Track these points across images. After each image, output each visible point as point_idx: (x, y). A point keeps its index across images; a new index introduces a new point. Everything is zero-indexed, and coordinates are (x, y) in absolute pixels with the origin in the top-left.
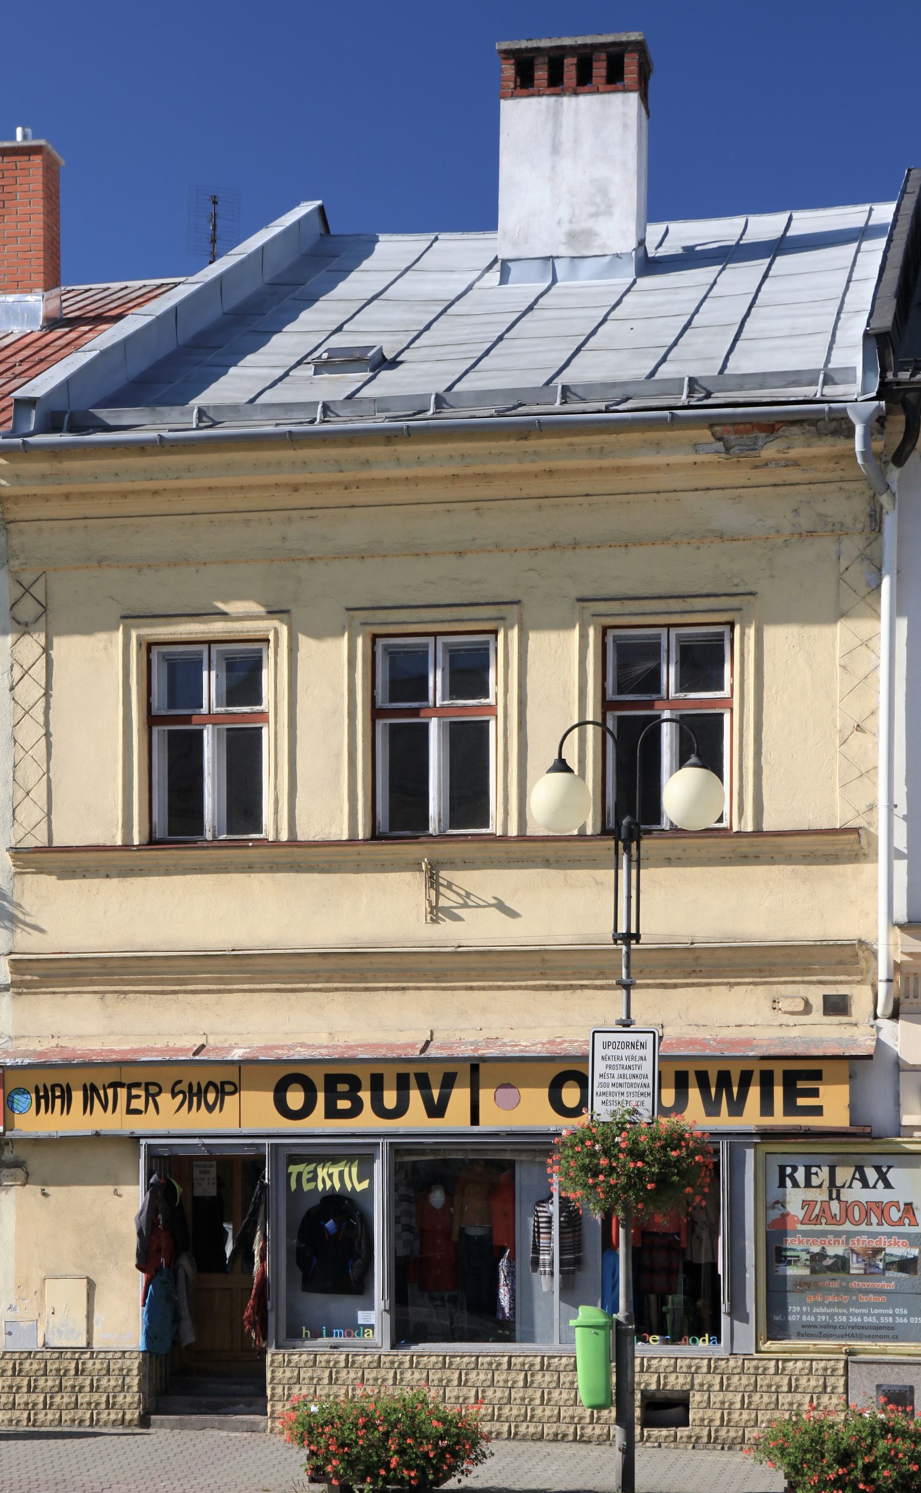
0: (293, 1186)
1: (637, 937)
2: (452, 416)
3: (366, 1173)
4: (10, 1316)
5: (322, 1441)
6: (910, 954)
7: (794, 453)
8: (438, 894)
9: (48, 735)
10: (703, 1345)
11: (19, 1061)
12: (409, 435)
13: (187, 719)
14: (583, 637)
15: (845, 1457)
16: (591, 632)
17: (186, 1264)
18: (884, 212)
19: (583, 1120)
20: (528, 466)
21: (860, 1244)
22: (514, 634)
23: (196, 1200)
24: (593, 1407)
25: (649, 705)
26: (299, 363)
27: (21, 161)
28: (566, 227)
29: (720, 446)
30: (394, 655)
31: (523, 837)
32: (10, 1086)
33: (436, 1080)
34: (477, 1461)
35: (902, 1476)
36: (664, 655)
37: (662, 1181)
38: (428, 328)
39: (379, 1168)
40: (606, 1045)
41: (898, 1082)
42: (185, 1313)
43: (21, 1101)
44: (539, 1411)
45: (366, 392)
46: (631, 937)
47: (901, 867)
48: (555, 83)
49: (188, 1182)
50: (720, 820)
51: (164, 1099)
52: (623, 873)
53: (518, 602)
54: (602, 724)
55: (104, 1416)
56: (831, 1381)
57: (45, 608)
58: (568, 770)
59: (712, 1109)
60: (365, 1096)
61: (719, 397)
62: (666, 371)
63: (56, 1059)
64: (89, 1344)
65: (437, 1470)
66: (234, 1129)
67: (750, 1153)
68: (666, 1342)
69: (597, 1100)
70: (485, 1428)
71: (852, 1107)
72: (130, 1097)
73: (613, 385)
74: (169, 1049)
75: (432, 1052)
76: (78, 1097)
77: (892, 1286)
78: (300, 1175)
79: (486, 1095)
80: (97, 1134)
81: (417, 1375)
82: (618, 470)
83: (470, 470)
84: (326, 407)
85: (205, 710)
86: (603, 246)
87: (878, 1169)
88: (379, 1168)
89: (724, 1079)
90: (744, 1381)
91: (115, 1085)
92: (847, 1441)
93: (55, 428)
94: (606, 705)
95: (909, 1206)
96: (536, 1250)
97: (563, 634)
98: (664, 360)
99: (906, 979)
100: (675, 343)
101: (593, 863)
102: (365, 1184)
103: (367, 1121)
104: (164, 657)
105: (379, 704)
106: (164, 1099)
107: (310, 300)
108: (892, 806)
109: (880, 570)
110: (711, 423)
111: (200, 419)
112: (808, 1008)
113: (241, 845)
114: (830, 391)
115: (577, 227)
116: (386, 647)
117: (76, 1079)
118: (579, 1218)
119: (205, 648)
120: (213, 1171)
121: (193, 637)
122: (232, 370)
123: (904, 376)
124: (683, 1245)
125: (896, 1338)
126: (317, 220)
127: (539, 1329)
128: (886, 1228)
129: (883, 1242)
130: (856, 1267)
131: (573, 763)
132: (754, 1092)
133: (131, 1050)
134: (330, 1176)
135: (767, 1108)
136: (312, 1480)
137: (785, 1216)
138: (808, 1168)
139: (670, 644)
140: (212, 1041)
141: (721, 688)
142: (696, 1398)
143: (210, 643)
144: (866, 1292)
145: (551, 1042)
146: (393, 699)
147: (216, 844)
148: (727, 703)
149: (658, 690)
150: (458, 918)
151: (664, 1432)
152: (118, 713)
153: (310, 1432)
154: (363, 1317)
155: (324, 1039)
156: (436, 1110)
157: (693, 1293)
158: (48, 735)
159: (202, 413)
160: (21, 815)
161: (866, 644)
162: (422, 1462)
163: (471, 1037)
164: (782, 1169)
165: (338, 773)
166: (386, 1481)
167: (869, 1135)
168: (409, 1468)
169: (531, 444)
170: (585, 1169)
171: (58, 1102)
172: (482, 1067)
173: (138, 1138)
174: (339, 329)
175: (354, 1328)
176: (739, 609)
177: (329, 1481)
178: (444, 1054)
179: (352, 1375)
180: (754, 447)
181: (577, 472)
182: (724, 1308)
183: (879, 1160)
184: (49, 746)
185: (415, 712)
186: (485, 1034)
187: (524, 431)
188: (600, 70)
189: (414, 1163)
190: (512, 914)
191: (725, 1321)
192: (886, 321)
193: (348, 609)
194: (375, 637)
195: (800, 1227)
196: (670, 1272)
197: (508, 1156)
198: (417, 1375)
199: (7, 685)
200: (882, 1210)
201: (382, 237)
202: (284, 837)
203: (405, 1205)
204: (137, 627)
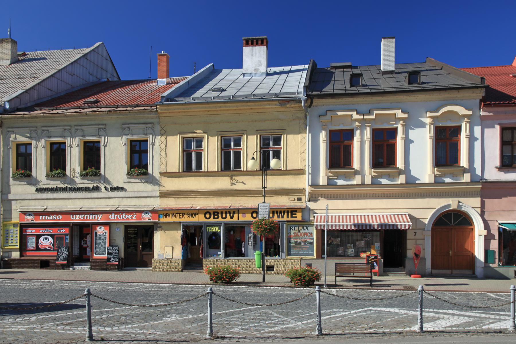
0: (207, 231)
1: (266, 188)
2: (235, 99)
3: (220, 229)
4: (159, 253)
5: (212, 274)
6: (312, 191)
7: (292, 106)
8: (232, 181)
9: (166, 153)
10: (277, 257)
11: (161, 209)
12: (228, 102)
13: (190, 151)
14: (257, 137)
15: (300, 275)
16: (258, 136)
17: (189, 244)
18: (307, 66)
19: (257, 219)
20: (248, 108)
21: (303, 240)
22: (245, 136)
23: (191, 233)
24: (258, 268)
25: (268, 148)
26: (209, 90)
27: (163, 57)
28: (254, 68)
29: (280, 104)
30: (225, 140)
31: (247, 171)
32: (159, 214)
33: (232, 212)
34: (239, 277)
35: (310, 278)
36: (270, 140)
37: (270, 229)
38: (231, 84)
39: (222, 228)
40: (261, 206)
41: (309, 212)
42: (189, 252)
43: (161, 216)
44: (249, 269)
45: (220, 95)
46: (265, 188)
47: (310, 176)
48: (252, 44)
49: (190, 230)
50: (280, 168)
51: (185, 216)
52: (264, 177)
53: (246, 131)
54: (260, 151)
55: (175, 270)
56: (298, 263)
57: (166, 132)
58: (254, 159)
59: (278, 217)
60: (220, 215)
61: (280, 96)
62: (271, 92)
63: (167, 209)
64: (173, 258)
65: (232, 279)
66: (197, 221)
67: (285, 225)
68: (270, 257)
69: (259, 216)
70: (240, 272)
71: (302, 217)
72: (180, 216)
73: (262, 94)
74: (186, 207)
75: (231, 208)
76: (171, 215)
77: (308, 247)
78: (208, 229)
79: (240, 215)
80: (174, 222)
81: (228, 263)
82: (263, 108)
83: (238, 108)
84: (214, 97)
85: (193, 149)
86: (260, 71)
87: (306, 227)
88: (222, 228)
89: (281, 212)
90: (284, 263)
91: (177, 213)
92: (301, 273)
93: (168, 101)
94: (261, 148)
95: (311, 233)
96: (249, 241)
97: (254, 136)
98: (270, 90)
99: (311, 195)
100: (272, 87)
101: (259, 175)
102: (220, 230)
103: (220, 219)
104: (186, 140)
105: (222, 148)
106: (185, 216)
107: (211, 80)
108: (309, 166)
109: (306, 125)
110: (278, 100)
111: (192, 100)
112: (295, 200)
113: (199, 172)
114: (298, 95)
115: (256, 68)
116: (223, 138)
117: (171, 212)
118: (256, 236)
119: (193, 138)
120: (194, 228)
121: (191, 137)
122: (198, 91)
123: (310, 93)
124: (274, 240)
125: (309, 256)
126: (212, 68)
127: (249, 254)
128: (307, 237)
129: (307, 239)
130: (302, 244)
131: (255, 158)
132: (286, 214)
133: (180, 208)
134: (214, 229)
135: (288, 217)
136: (210, 280)
137: (291, 235)
138: (295, 227)
139: (272, 138)
140: (194, 206)
141: (280, 145)
142: (275, 266)
143: (194, 137)
144: (304, 248)
145: (251, 206)
146: (225, 147)
147: (194, 172)
148: (281, 148)
149: (270, 146)
150: (235, 185)
151: (270, 272)
152: (385, 56)
153: (210, 272)
154: (219, 253)
155: (213, 205)
156: (232, 218)
157: (275, 248)
158: (166, 153)
159: (193, 98)
160: (161, 167)
161: (304, 138)
162: (229, 277)
163: (238, 205)
164: (290, 227)
165: (215, 160)
166: (223, 280)
167: (305, 221)
168: (227, 278)
169: (248, 104)
170: (257, 227)
171: (167, 216)
172: (240, 210)
173: (181, 222)
174: (216, 85)
175: (218, 255)
176: (283, 132)
177: (213, 281)
178: (233, 208)
179: (217, 263)
180: (285, 105)
181: (256, 109)
182: (280, 251)
183: (306, 226)
184: (166, 155)
185: (228, 149)
186: (240, 205)
187: (247, 102)
188: (260, 42)
189: (228, 227)
190: (245, 184)
191: (280, 253)
192: (307, 84)
193: (217, 132)
194: (222, 137)
195: (293, 237)
196: (271, 245)
197: (244, 225)
198: (228, 263)
199: (159, 145)
200: (307, 234)
201: (223, 70)
202: (206, 171)
203: (226, 234)
204: (181, 135)
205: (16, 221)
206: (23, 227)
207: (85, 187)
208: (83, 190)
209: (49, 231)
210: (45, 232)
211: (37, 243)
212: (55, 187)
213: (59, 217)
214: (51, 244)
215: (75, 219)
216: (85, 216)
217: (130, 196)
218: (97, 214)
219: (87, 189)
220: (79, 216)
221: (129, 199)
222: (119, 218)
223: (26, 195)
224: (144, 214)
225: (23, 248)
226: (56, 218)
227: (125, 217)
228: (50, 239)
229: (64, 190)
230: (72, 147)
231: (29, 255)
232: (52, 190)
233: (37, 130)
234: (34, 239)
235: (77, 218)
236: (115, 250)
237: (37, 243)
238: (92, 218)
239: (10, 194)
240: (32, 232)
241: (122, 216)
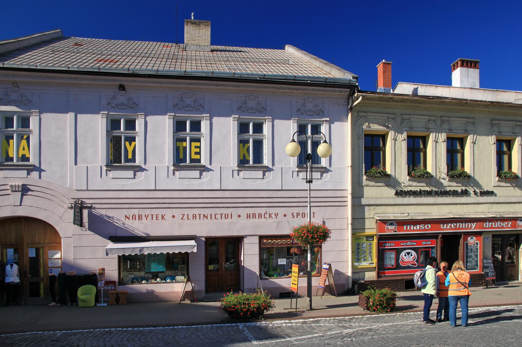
205: (373, 232)
206: (383, 239)
207: (454, 191)
208: (410, 195)
209: (412, 244)
210: (407, 245)
211: (397, 258)
212: (419, 190)
213: (428, 227)
214: (414, 260)
215: (447, 229)
216: (457, 225)
217: (501, 201)
218: (470, 223)
219: (455, 193)
220: (451, 225)
221: (498, 205)
222: (494, 226)
223: (383, 200)
224: (519, 222)
225: (381, 267)
226: (423, 228)
227: (500, 225)
228: (414, 253)
229: (429, 194)
230: (438, 143)
231: (389, 275)
232: (414, 194)
233: (396, 118)
234: (393, 255)
235: (448, 227)
236: (490, 263)
237: (397, 258)
238: (465, 227)
239: (363, 197)
240: (390, 246)
241: (497, 223)
